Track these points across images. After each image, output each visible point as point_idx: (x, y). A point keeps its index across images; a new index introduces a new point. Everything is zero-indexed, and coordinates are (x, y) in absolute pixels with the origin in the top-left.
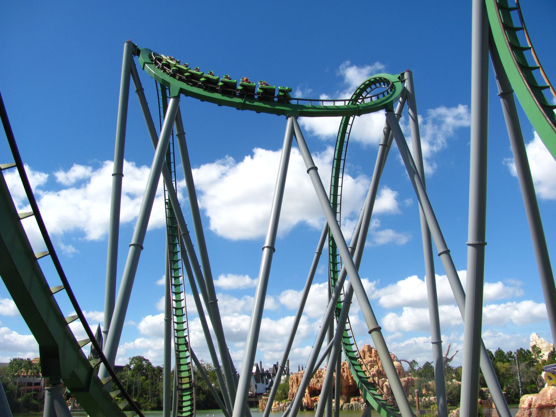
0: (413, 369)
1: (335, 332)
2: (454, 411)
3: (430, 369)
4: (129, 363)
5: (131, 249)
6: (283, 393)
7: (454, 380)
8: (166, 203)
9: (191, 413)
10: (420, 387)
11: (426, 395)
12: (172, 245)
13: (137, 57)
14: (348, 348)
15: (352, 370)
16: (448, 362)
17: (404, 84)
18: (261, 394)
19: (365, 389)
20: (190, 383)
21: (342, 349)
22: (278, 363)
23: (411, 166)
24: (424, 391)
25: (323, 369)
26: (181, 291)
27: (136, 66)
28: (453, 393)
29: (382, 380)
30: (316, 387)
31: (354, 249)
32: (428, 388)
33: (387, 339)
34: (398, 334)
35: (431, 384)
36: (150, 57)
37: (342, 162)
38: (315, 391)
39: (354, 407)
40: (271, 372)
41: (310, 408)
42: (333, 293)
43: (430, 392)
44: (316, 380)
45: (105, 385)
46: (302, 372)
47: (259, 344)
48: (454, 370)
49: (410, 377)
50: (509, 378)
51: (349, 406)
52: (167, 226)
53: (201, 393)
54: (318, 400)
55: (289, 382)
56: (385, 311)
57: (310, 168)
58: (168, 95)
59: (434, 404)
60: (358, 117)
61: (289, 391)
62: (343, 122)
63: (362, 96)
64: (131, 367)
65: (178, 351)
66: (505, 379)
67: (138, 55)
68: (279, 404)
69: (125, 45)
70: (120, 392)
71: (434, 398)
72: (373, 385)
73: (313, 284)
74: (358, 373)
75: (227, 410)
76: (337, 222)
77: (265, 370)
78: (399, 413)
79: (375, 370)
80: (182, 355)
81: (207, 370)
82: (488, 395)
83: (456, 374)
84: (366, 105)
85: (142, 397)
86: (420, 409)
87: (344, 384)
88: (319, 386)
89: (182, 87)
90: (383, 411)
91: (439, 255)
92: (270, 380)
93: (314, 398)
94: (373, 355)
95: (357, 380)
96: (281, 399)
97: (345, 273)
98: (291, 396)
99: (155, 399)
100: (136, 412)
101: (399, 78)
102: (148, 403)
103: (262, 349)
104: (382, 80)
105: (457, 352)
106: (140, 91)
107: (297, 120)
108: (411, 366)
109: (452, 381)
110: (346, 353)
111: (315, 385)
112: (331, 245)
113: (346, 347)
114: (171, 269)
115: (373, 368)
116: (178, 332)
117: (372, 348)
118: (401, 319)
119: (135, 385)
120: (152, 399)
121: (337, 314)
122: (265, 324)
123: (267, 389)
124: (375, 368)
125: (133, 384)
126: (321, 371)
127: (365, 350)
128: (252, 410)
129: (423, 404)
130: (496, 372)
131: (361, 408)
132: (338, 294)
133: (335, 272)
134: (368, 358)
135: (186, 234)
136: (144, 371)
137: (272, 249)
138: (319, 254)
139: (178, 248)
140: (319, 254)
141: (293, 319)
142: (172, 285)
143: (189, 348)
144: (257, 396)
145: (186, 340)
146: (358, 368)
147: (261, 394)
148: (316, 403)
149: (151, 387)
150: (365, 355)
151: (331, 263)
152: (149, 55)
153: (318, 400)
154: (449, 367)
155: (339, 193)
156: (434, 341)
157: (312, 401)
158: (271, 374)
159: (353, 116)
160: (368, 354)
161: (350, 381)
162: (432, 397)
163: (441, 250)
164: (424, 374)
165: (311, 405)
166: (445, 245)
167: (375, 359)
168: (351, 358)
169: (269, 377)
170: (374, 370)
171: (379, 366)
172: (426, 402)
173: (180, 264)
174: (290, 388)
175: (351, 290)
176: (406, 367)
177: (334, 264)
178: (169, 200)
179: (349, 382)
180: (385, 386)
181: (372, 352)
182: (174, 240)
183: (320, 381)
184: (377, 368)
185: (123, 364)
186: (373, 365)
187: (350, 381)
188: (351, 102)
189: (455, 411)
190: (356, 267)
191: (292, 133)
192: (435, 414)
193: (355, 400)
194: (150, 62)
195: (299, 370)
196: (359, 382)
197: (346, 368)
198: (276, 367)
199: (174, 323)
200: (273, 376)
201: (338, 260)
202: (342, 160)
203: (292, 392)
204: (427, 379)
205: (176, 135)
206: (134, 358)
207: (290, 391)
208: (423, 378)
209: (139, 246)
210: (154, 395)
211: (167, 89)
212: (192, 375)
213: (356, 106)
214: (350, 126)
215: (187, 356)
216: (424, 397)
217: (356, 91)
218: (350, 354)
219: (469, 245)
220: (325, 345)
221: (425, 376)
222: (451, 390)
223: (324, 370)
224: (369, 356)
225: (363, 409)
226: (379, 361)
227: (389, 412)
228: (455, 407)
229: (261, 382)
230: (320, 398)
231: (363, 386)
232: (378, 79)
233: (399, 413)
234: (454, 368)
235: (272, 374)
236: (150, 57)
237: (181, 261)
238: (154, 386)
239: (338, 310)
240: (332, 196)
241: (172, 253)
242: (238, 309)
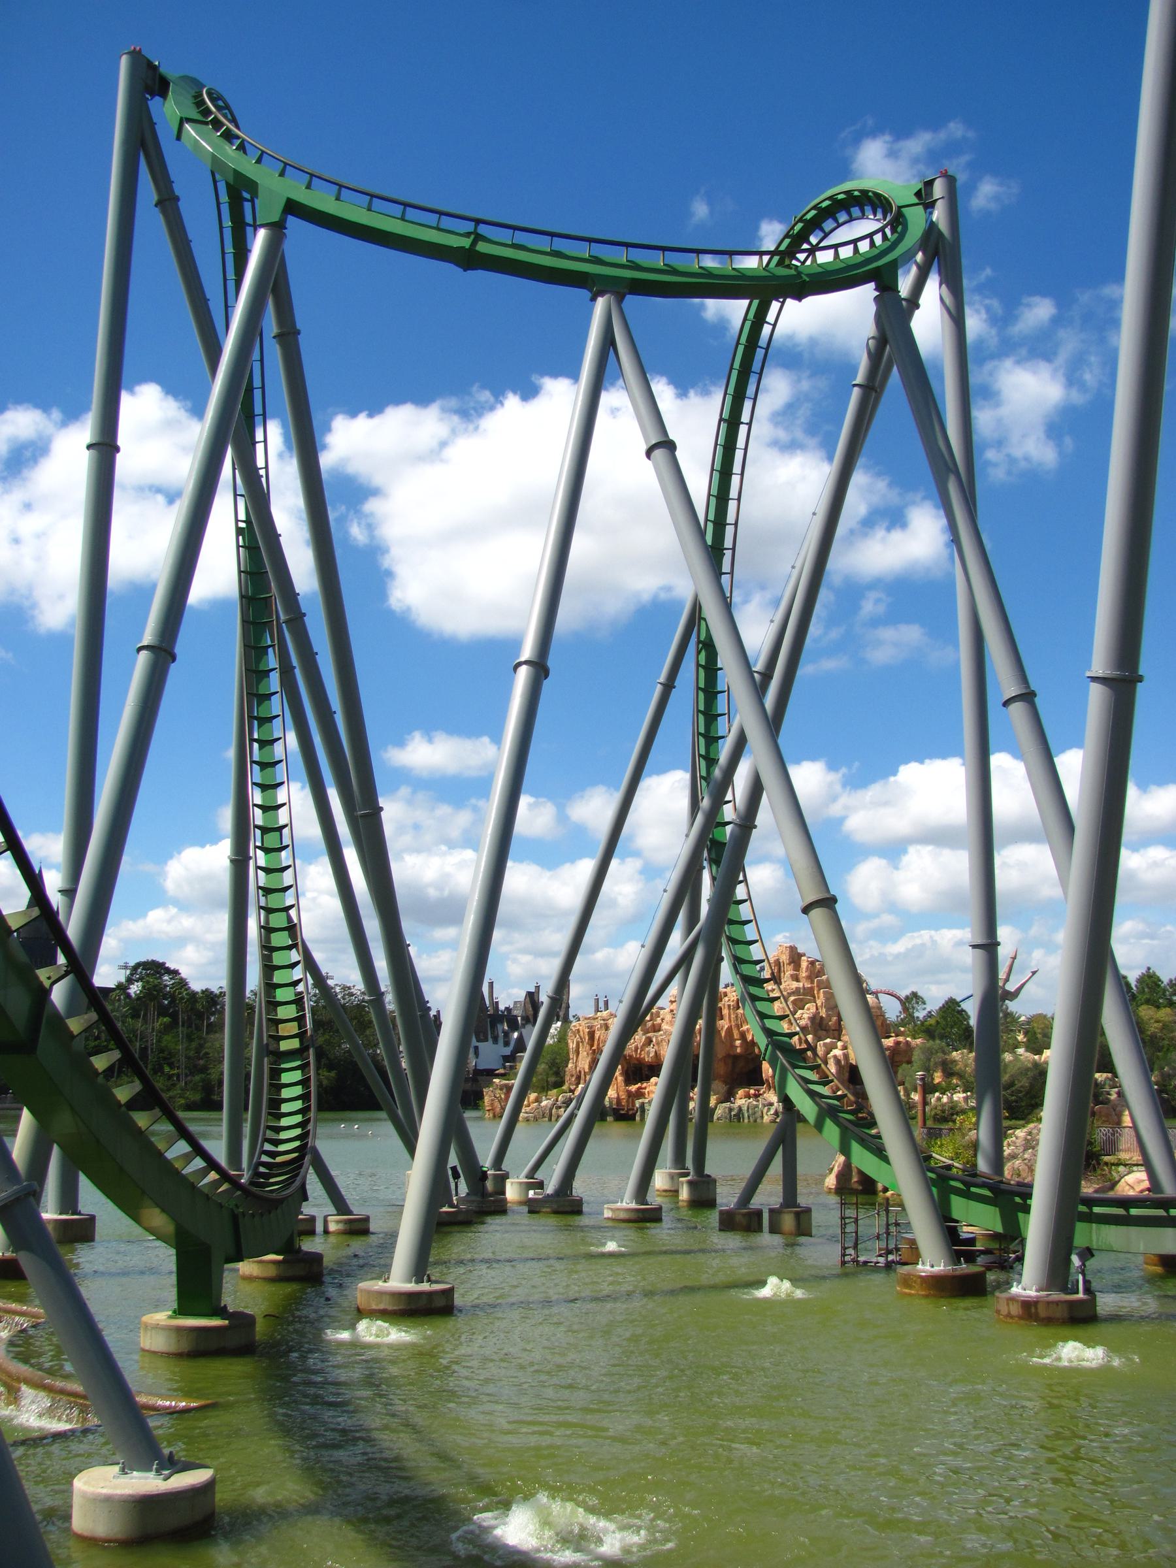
0: (911, 1016)
1: (704, 909)
2: (1019, 1132)
3: (958, 1018)
4: (123, 980)
5: (143, 659)
6: (551, 1072)
7: (1021, 1051)
8: (239, 531)
9: (303, 1117)
10: (929, 1066)
11: (942, 1088)
12: (253, 651)
13: (157, 99)
14: (740, 951)
15: (747, 1011)
16: (1007, 1002)
17: (931, 213)
18: (491, 1073)
19: (782, 1064)
20: (301, 1035)
21: (724, 954)
22: (538, 988)
23: (940, 450)
24: (938, 1078)
25: (662, 1008)
26: (278, 781)
27: (156, 127)
28: (1018, 1085)
29: (824, 1044)
30: (642, 1056)
31: (767, 675)
32: (949, 1071)
33: (855, 931)
34: (887, 919)
35: (957, 1058)
36: (200, 103)
37: (743, 429)
38: (641, 1069)
39: (746, 1115)
40: (517, 1012)
41: (626, 1115)
42: (703, 798)
43: (955, 1081)
44: (644, 1037)
45: (77, 1035)
46: (605, 1014)
47: (497, 935)
48: (1023, 1025)
49: (901, 1039)
50: (1168, 1049)
51: (731, 1110)
52: (242, 597)
53: (324, 1064)
54: (646, 1091)
55: (569, 1041)
56: (857, 852)
57: (654, 442)
58: (249, 219)
59: (963, 1112)
60: (796, 302)
61: (567, 1066)
62: (751, 316)
63: (809, 243)
64: (129, 991)
65: (268, 949)
66: (1159, 1052)
67: (163, 92)
68: (538, 1100)
69: (124, 61)
70: (119, 1056)
71: (964, 1097)
72: (797, 1057)
73: (650, 775)
74: (766, 1021)
75: (400, 1112)
76: (724, 597)
77: (502, 1007)
78: (874, 1132)
79: (806, 1016)
80: (278, 958)
81: (342, 1001)
82: (1109, 1094)
83: (1026, 1034)
84: (820, 270)
85: (159, 1074)
86: (927, 1126)
87: (720, 1052)
88: (651, 1056)
89: (295, 196)
90: (829, 1125)
91: (1006, 704)
92: (516, 1035)
93: (637, 1086)
94: (803, 974)
95: (762, 1041)
96: (544, 1089)
97: (741, 742)
98: (573, 1079)
99: (197, 1078)
100: (162, 1110)
101: (918, 194)
102: (176, 1092)
103: (505, 949)
104: (869, 198)
105: (1034, 973)
106: (168, 202)
107: (623, 305)
108: (905, 1009)
109: (1015, 1053)
110: (734, 965)
111: (641, 1051)
112: (704, 664)
113: (735, 950)
114: (251, 718)
115: (803, 1009)
116: (269, 896)
117: (800, 955)
118: (899, 876)
119: (141, 1039)
120: (189, 1078)
121: (713, 856)
122: (517, 878)
123: (506, 1059)
124: (808, 1009)
125: (137, 1037)
126: (658, 1015)
127: (781, 961)
128: (468, 1114)
129: (933, 1113)
130: (1137, 1028)
131: (766, 1117)
132: (718, 801)
133: (712, 740)
134: (787, 983)
135: (297, 619)
136: (166, 1002)
137: (540, 668)
138: (669, 686)
139: (272, 661)
140: (669, 686)
141: (586, 868)
142: (253, 762)
143: (299, 940)
144: (480, 1078)
145: (290, 919)
146: (761, 1006)
147: (491, 1073)
148: (640, 1101)
149: (185, 1046)
150: (782, 974)
151: (700, 714)
152: (195, 97)
153: (646, 1091)
154: (1008, 1014)
155: (731, 518)
156: (979, 941)
157: (629, 1094)
158: (519, 1018)
159: (781, 300)
160: (789, 971)
161: (738, 1043)
162: (958, 1095)
163: (1012, 690)
164: (939, 1031)
165: (628, 1106)
166: (1023, 678)
167: (809, 986)
168: (748, 980)
169: (514, 1025)
170: (805, 1015)
171: (819, 1004)
172: (943, 1105)
173: (277, 705)
174: (571, 1057)
175: (756, 789)
176: (892, 1010)
177: (710, 716)
178: (248, 521)
179: (734, 1047)
180: (832, 1060)
181: (799, 965)
182: (259, 637)
183: (654, 1040)
184: (813, 1010)
185: (111, 984)
186: (801, 1000)
187: (738, 1043)
188: (776, 259)
189: (1020, 1133)
190: (774, 723)
191: (608, 343)
192: (967, 1138)
193: (748, 1096)
194: (199, 117)
195: (597, 1010)
196: (767, 1046)
197: (726, 1006)
198: (532, 998)
199: (259, 871)
200: (524, 1022)
201: (721, 705)
202: (742, 423)
203: (576, 1067)
204: (948, 1045)
205: (274, 337)
206: (138, 965)
207: (570, 1065)
208: (938, 1042)
209: (165, 651)
210: (194, 1069)
211: (247, 200)
212: (307, 1015)
213: (793, 272)
214: (771, 327)
215: (293, 961)
216: (937, 1094)
217: (792, 228)
218: (747, 970)
219: (1094, 679)
220: (676, 943)
221: (942, 1037)
222: (1012, 1076)
223: (668, 1010)
224: (792, 976)
225: (768, 1121)
226: (818, 993)
227: (846, 1128)
228: (1021, 1122)
229: (490, 1040)
230: (655, 1088)
231: (778, 1058)
232: (856, 193)
233: (874, 1132)
234: (1023, 1018)
235: (522, 1019)
236: (200, 103)
237: (278, 695)
238: (194, 1045)
239: (717, 847)
240: (710, 526)
241: (254, 674)
242: (455, 833)
